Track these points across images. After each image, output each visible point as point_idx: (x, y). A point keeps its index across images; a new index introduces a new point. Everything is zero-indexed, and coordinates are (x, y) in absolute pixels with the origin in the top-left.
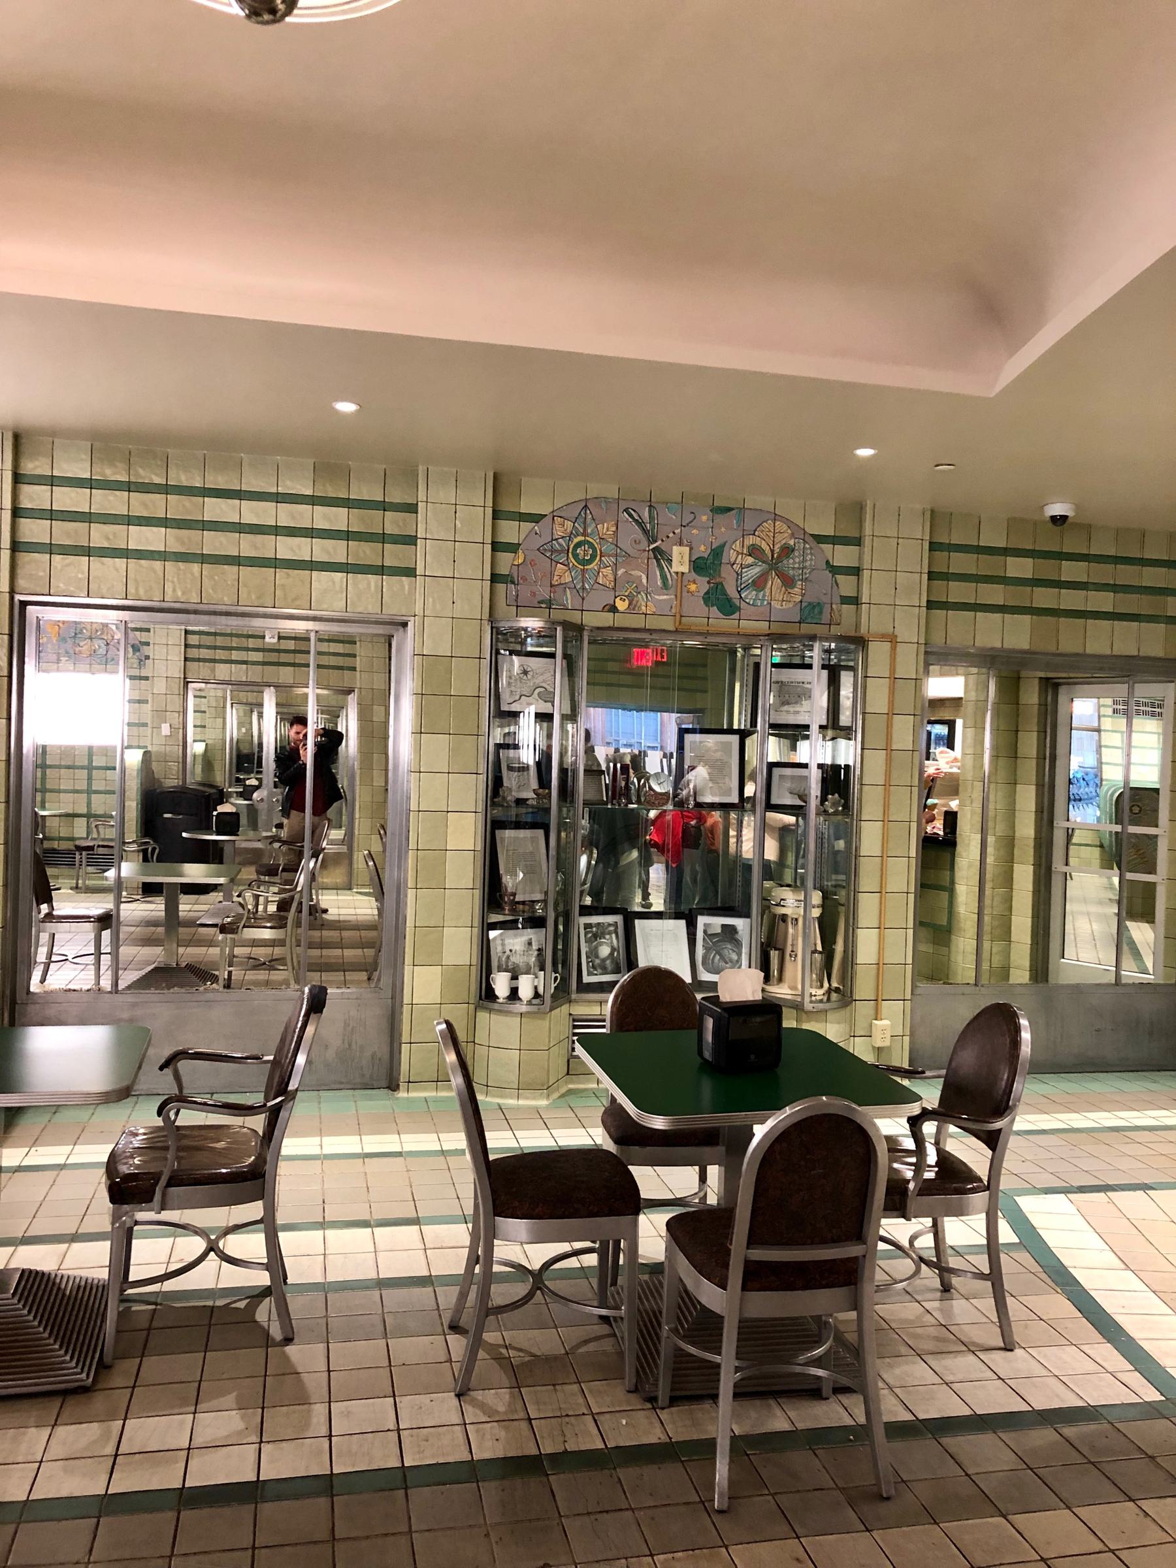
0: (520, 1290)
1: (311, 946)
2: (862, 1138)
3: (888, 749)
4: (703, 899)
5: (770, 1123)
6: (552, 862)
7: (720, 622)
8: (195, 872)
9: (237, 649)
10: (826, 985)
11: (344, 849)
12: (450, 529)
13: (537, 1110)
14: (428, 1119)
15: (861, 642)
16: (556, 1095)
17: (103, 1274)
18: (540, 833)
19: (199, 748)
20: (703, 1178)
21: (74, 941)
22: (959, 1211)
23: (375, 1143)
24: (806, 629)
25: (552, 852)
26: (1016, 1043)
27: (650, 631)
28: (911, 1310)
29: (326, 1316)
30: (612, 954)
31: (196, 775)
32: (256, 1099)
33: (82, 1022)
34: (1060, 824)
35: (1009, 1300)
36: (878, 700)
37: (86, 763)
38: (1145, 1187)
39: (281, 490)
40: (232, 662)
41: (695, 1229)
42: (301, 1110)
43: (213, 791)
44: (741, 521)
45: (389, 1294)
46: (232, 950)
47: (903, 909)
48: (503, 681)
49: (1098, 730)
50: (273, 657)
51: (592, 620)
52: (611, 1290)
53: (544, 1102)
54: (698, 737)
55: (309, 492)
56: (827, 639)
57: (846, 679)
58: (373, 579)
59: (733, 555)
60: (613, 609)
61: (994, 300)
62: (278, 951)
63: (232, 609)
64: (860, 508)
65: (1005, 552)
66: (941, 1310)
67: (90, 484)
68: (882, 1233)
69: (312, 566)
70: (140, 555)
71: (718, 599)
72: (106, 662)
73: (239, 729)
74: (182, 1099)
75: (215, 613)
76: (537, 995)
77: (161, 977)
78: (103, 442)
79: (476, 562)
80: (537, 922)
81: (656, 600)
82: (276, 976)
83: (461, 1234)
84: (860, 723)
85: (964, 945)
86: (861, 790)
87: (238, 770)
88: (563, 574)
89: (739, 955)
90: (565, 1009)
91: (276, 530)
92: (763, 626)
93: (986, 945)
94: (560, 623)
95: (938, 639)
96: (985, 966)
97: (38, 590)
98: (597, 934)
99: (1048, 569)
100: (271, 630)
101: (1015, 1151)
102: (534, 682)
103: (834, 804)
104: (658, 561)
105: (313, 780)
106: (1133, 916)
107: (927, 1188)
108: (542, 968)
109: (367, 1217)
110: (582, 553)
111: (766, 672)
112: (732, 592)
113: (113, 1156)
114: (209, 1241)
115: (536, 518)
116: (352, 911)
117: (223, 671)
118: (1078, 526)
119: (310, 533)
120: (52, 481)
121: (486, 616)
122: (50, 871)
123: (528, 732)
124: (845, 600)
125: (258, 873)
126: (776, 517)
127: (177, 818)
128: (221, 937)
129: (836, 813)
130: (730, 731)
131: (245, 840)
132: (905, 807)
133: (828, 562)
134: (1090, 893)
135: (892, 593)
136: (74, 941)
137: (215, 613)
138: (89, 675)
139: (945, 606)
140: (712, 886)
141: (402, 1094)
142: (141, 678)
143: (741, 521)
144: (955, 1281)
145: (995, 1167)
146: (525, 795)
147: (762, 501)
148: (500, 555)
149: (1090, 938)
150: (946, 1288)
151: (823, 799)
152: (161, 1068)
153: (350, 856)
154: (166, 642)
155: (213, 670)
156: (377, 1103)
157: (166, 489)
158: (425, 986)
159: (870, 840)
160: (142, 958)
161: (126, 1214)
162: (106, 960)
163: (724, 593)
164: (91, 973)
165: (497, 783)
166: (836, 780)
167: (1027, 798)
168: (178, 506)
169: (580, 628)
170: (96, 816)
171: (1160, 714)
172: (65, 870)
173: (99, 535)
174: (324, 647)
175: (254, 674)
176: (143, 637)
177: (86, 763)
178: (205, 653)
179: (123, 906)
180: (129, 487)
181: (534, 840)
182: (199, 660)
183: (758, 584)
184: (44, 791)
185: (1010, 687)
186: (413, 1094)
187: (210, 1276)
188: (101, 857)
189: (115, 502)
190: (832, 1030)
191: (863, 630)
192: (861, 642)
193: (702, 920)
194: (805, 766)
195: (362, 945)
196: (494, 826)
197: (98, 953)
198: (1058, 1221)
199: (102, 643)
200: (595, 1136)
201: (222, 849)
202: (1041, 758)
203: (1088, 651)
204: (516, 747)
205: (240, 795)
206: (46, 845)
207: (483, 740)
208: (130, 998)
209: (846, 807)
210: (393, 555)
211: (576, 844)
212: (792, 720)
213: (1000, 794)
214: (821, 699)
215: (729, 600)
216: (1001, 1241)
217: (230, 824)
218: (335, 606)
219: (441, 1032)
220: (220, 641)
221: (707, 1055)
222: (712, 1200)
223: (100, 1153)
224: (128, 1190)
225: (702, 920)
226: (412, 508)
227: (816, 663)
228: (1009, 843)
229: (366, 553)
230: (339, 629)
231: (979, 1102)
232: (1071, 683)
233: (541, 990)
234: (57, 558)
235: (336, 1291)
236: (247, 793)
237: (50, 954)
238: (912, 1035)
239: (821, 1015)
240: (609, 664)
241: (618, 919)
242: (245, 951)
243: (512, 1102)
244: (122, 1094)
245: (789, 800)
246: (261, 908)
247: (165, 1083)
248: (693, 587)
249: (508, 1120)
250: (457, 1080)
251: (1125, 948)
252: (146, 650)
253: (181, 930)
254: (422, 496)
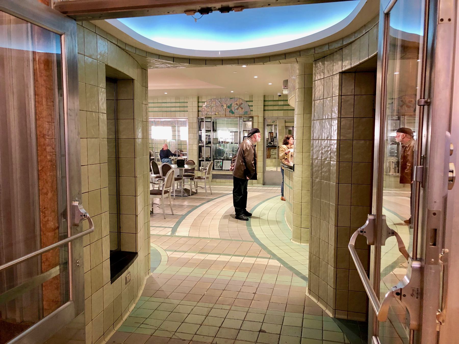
65: (278, 101)
92: (238, 116)
183: (237, 109)
229: (182, 109)
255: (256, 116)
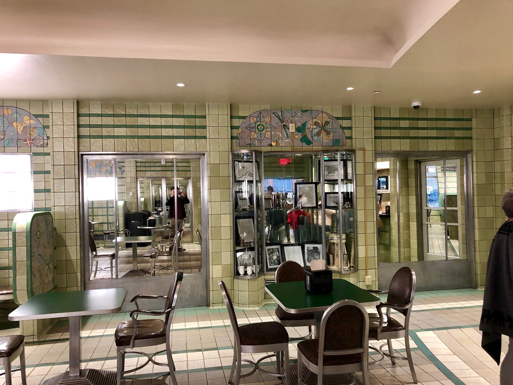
0: (252, 369)
1: (179, 261)
2: (360, 314)
3: (365, 186)
4: (308, 239)
5: (329, 309)
6: (256, 229)
7: (306, 147)
8: (143, 239)
9: (152, 167)
10: (349, 265)
11: (190, 229)
12: (217, 122)
13: (255, 311)
14: (219, 316)
15: (353, 151)
16: (262, 306)
17: (115, 370)
18: (252, 219)
19: (142, 199)
20: (310, 330)
21: (104, 264)
22: (396, 337)
23: (202, 324)
24: (335, 148)
25: (256, 225)
26: (411, 279)
27: (284, 152)
28: (382, 371)
29: (188, 381)
30: (277, 258)
31: (141, 208)
32: (162, 311)
33: (107, 288)
34: (424, 208)
35: (415, 367)
36: (360, 170)
37: (106, 206)
38: (460, 327)
39: (162, 114)
40: (151, 171)
41: (307, 346)
42: (176, 314)
43: (147, 213)
44: (311, 114)
45: (210, 374)
46: (155, 264)
47: (373, 239)
48: (237, 171)
49: (437, 177)
50: (164, 168)
51: (264, 149)
52: (281, 368)
53: (258, 308)
54: (302, 186)
55: (171, 114)
56: (342, 151)
57: (349, 164)
58: (193, 140)
59: (309, 125)
60: (271, 145)
61: (388, 36)
62: (170, 263)
63: (149, 153)
64: (350, 107)
65: (399, 119)
66: (392, 371)
67: (101, 115)
68: (370, 345)
69: (173, 137)
70: (118, 137)
71: (305, 140)
72: (109, 173)
73: (155, 193)
74: (138, 311)
75: (143, 154)
76: (253, 273)
77: (132, 273)
78: (105, 102)
79: (226, 133)
80: (252, 249)
81: (285, 141)
82: (169, 271)
83: (231, 352)
84: (354, 177)
85: (394, 250)
86: (356, 200)
87: (156, 206)
88: (254, 135)
89: (319, 257)
90: (263, 277)
91: (161, 127)
92: (320, 148)
93: (402, 250)
94: (254, 151)
95: (379, 149)
96: (402, 257)
97: (87, 150)
98: (272, 252)
99: (414, 124)
100: (163, 159)
101: (413, 318)
102: (247, 170)
103: (348, 205)
104: (285, 129)
105: (179, 207)
106: (452, 238)
107: (384, 330)
108: (254, 264)
109: (201, 348)
110: (260, 128)
111: (323, 163)
112: (310, 137)
113: (117, 332)
114: (149, 357)
115: (244, 118)
116: (193, 249)
117: (148, 174)
118: (423, 109)
119: (172, 127)
120: (89, 115)
121: (230, 150)
122: (96, 242)
123: (245, 187)
124: (347, 138)
125: (162, 238)
126: (323, 112)
127: (136, 221)
128: (151, 259)
129: (349, 208)
130: (312, 183)
131: (158, 228)
132: (371, 204)
133: (341, 126)
134: (436, 231)
135: (362, 134)
136: (104, 264)
137: (143, 154)
138: (105, 178)
139: (381, 138)
140: (310, 234)
141: (211, 308)
142: (122, 178)
143: (311, 114)
144: (396, 361)
145: (407, 321)
146: (245, 207)
147: (319, 107)
148: (233, 130)
149: (437, 246)
150: (394, 364)
151: (344, 204)
152: (131, 302)
153: (192, 232)
154: (130, 165)
155: (145, 174)
156: (203, 311)
157: (126, 116)
158: (217, 272)
159: (360, 216)
160: (125, 268)
161: (122, 349)
162: (114, 269)
163: (307, 138)
164: (110, 274)
165: (236, 204)
166: (348, 197)
167: (413, 200)
168: (130, 121)
169: (261, 152)
170: (110, 223)
171: (455, 171)
172: (100, 241)
173: (105, 132)
174: (179, 164)
175: (159, 174)
176: (122, 164)
177: (106, 206)
178: (142, 169)
179: (120, 252)
180: (114, 116)
181: (249, 222)
182: (141, 171)
183: (318, 134)
184: (93, 216)
185: (405, 163)
186: (214, 308)
187: (149, 369)
188: (111, 236)
189: (109, 121)
190: (352, 280)
191: (354, 147)
192: (353, 151)
193: (306, 246)
194: (337, 193)
195: (197, 260)
196: (236, 218)
197: (112, 267)
198: (430, 339)
199: (109, 167)
200: (273, 318)
201: (151, 232)
202: (417, 186)
203: (429, 150)
204: (242, 192)
205: (156, 214)
206: (95, 233)
207: (231, 190)
208: (122, 281)
209: (352, 206)
210: (199, 132)
211: (266, 223)
212: (332, 178)
213: (404, 199)
214: (342, 172)
215: (309, 140)
216: (411, 347)
217: (153, 223)
218: (182, 150)
219: (220, 285)
220: (147, 164)
221: (308, 289)
222: (313, 338)
223: (113, 331)
224: (122, 341)
225: (306, 246)
226: (204, 117)
227: (339, 159)
228: (408, 216)
229: (190, 132)
230: (206, 170)
231: (400, 300)
232: (425, 161)
233: (254, 271)
234: (92, 140)
235: (191, 372)
236: (158, 214)
237: (97, 268)
238: (379, 280)
239: (348, 275)
240: (271, 163)
241: (279, 247)
242: (159, 264)
243: (247, 309)
244: (118, 310)
245: (333, 205)
246: (164, 250)
247: (132, 307)
248: (297, 137)
249: (246, 314)
250: (226, 301)
251: (449, 249)
252: (124, 169)
253: (138, 258)
254: (207, 113)
255: (361, 149)
